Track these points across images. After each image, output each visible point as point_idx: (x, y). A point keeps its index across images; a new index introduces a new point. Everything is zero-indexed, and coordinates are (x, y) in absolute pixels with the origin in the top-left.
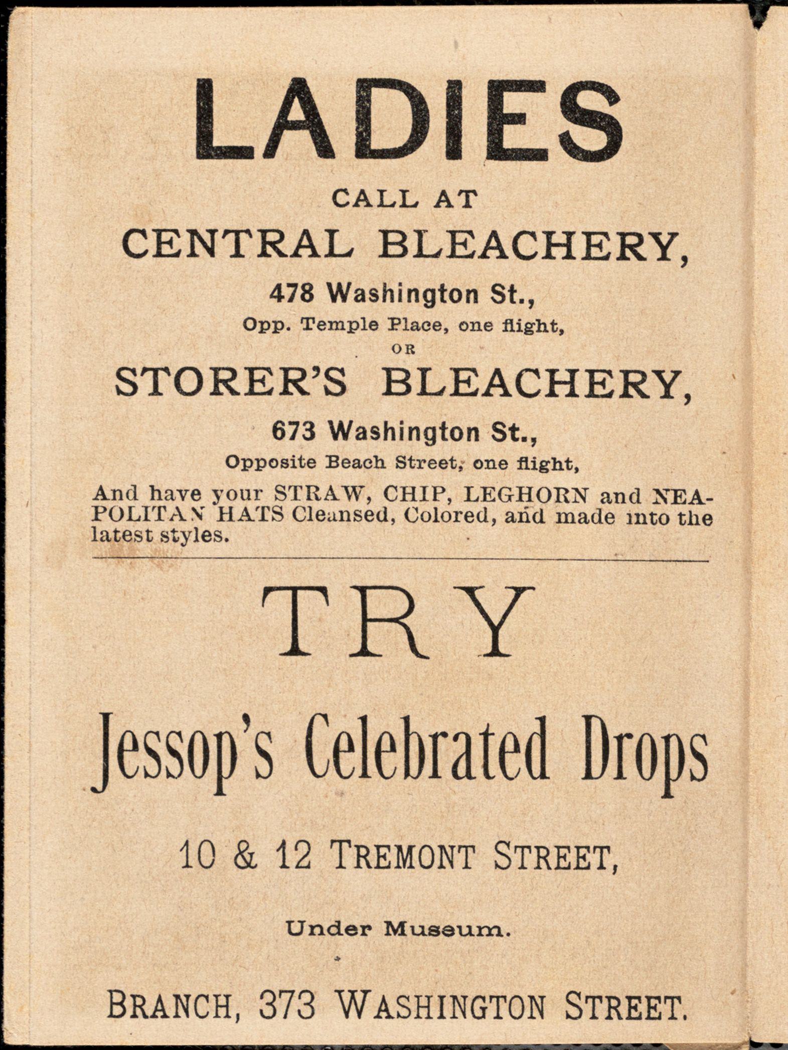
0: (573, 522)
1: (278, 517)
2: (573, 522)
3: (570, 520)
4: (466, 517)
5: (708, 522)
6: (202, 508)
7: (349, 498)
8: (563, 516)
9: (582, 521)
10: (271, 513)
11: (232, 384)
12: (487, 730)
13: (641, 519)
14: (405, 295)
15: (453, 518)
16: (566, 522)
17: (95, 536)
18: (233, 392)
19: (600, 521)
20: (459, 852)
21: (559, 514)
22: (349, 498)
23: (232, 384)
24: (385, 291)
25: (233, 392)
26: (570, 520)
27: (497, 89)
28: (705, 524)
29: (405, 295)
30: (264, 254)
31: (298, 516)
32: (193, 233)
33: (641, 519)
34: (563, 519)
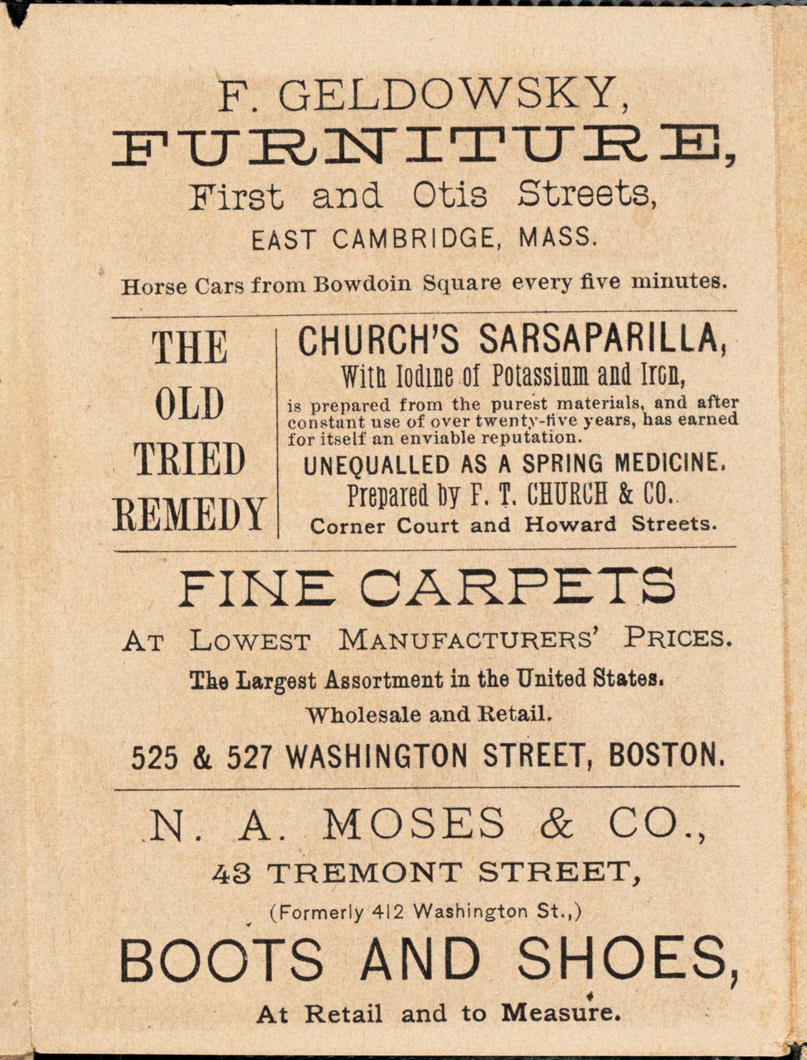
0: (649, 286)
1: (239, 290)
2: (649, 286)
3: (645, 284)
4: (492, 284)
5: (496, 286)
6: (590, 997)
7: (314, 719)
8: (639, 281)
9: (216, 290)
10: (247, 198)
11: (321, 1015)
12: (431, 579)
13: (668, 283)
14: (472, 912)
15: (155, 290)
16: (642, 286)
17: (318, 287)
18: (321, 1020)
19: (373, 288)
20: (536, 498)
21: (635, 279)
22: (314, 719)
23: (321, 1015)
24: (458, 910)
25: (321, 1020)
26: (645, 284)
27: (635, 455)
28: (533, 1019)
29: (472, 912)
30: (310, 1021)
31: (202, 290)
32: (355, 866)
33: (668, 283)
34: (639, 284)
